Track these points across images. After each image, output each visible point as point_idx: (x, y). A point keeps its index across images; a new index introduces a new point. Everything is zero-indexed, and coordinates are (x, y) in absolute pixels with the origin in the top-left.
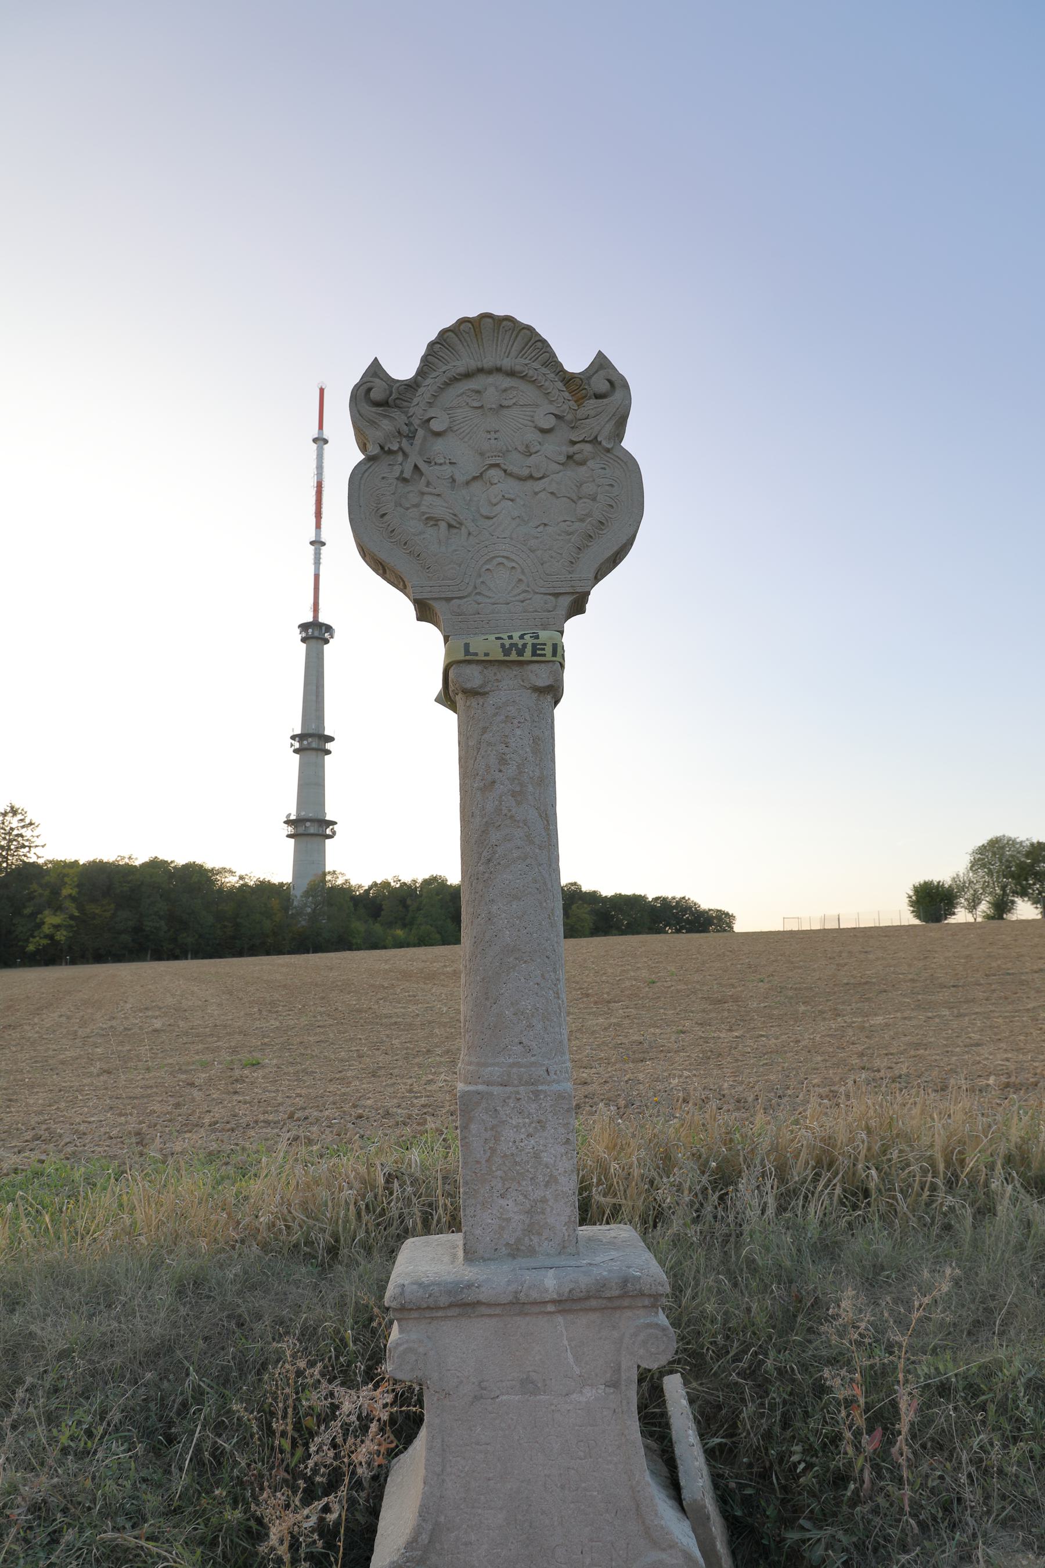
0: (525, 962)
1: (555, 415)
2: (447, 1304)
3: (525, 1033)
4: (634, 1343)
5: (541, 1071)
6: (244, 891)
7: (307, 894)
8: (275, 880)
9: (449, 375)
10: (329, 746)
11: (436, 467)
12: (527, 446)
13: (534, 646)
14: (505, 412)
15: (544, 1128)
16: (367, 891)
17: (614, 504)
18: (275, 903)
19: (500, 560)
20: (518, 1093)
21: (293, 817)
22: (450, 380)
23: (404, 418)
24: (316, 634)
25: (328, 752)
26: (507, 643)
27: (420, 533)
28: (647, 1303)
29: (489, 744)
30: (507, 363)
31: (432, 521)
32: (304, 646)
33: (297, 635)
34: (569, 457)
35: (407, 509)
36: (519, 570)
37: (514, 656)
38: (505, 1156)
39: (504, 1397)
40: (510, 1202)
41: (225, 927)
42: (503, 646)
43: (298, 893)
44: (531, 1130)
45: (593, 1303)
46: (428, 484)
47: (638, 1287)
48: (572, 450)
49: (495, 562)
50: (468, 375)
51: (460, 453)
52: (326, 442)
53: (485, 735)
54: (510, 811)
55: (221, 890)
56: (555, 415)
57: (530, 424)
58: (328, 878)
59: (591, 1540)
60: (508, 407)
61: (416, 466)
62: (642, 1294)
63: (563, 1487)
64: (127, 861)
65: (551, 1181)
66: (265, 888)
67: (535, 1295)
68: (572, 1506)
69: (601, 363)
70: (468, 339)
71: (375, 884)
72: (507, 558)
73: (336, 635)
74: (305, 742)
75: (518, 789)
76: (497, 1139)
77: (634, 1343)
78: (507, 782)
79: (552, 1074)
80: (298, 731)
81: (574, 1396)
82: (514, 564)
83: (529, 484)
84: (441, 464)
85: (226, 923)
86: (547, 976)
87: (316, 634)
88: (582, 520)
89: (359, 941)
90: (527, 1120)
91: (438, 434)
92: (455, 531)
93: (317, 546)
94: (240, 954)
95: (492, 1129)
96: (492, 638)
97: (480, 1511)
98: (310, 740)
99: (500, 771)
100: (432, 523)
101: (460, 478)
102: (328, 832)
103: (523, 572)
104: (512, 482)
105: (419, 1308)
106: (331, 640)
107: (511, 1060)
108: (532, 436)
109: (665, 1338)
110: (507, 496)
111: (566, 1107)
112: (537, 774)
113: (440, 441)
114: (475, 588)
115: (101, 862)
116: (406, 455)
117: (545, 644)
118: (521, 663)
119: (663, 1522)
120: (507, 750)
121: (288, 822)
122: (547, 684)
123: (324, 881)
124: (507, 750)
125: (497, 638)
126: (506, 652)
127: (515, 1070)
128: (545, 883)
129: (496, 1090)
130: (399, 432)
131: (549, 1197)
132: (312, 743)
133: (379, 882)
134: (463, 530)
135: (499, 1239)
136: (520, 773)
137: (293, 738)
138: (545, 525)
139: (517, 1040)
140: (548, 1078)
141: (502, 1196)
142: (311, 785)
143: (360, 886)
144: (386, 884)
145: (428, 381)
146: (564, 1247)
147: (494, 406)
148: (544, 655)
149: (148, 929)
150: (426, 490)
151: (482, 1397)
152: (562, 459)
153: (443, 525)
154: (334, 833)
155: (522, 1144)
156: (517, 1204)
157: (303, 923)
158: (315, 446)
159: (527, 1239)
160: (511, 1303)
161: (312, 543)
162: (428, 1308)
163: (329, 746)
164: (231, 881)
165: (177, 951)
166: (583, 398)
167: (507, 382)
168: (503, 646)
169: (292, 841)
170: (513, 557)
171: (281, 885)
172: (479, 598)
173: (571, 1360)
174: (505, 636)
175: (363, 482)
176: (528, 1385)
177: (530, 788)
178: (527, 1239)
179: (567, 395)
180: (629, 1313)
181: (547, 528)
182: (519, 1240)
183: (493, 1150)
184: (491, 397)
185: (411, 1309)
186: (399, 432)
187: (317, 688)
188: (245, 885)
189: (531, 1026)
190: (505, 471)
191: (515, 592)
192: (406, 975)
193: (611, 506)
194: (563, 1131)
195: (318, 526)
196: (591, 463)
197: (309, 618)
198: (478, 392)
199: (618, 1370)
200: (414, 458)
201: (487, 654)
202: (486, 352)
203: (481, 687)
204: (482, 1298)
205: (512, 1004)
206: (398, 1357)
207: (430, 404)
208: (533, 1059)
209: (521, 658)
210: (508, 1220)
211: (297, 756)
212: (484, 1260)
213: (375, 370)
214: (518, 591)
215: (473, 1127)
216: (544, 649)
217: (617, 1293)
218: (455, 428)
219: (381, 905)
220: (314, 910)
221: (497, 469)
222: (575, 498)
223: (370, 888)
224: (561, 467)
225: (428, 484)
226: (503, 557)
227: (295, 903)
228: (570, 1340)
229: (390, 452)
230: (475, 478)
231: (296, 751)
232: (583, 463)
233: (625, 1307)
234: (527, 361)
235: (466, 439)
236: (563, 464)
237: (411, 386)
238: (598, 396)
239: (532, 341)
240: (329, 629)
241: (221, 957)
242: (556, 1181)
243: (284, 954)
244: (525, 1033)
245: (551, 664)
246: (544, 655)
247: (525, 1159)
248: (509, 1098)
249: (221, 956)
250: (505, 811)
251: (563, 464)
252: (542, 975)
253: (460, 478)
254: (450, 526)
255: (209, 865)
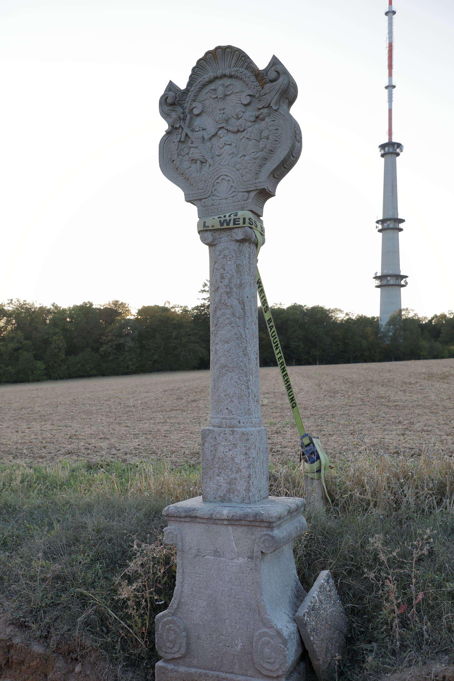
0: (230, 372)
1: (250, 95)
2: (184, 516)
3: (229, 404)
4: (259, 541)
5: (236, 422)
6: (349, 323)
7: (389, 323)
8: (369, 315)
9: (201, 83)
10: (401, 226)
11: (196, 133)
12: (237, 115)
13: (234, 219)
14: (228, 98)
15: (236, 447)
16: (430, 321)
17: (278, 139)
18: (369, 329)
19: (223, 177)
20: (225, 431)
21: (379, 274)
22: (203, 86)
23: (181, 110)
24: (391, 150)
25: (401, 230)
26: (222, 220)
27: (189, 168)
28: (266, 525)
29: (217, 269)
30: (227, 72)
31: (194, 161)
32: (383, 159)
33: (378, 152)
34: (257, 117)
35: (184, 156)
36: (232, 181)
37: (225, 226)
38: (219, 458)
39: (207, 557)
40: (221, 478)
41: (338, 345)
42: (220, 221)
43: (383, 323)
44: (231, 448)
45: (243, 522)
46: (192, 143)
47: (261, 518)
48: (258, 113)
49: (221, 178)
50: (211, 81)
51: (208, 123)
52: (394, 13)
53: (216, 265)
54: (225, 301)
55: (335, 323)
56: (250, 95)
57: (239, 102)
58: (403, 313)
59: (240, 619)
60: (229, 95)
61: (186, 134)
62: (262, 521)
63: (229, 596)
64: (279, 306)
65: (239, 471)
66: (363, 321)
67: (218, 516)
68: (233, 604)
69: (275, 62)
70: (211, 62)
71: (436, 316)
72: (227, 175)
73: (404, 149)
74: (385, 225)
75: (229, 290)
76: (216, 450)
77: (259, 541)
78: (224, 287)
79: (242, 423)
80: (381, 218)
81: (235, 560)
82: (229, 178)
83: (239, 134)
84: (198, 131)
85: (339, 343)
86: (241, 378)
87: (391, 150)
88: (262, 151)
89: (425, 354)
90: (229, 443)
91: (198, 115)
92: (204, 164)
93: (390, 88)
94: (348, 361)
95: (214, 446)
96: (216, 217)
97: (197, 600)
98: (389, 222)
99: (221, 282)
100: (194, 162)
101: (207, 137)
102: (403, 282)
103: (233, 182)
104: (231, 135)
105: (174, 516)
106: (401, 154)
107: (223, 416)
108: (240, 108)
109: (272, 541)
110: (226, 143)
111: (246, 438)
112: (238, 282)
113: (199, 119)
114: (212, 192)
115: (85, 311)
116: (182, 129)
117: (239, 219)
118: (230, 229)
119: (268, 617)
120: (224, 272)
121: (376, 278)
122: (241, 238)
123: (400, 315)
124: (224, 272)
125: (219, 218)
126: (222, 224)
127: (224, 421)
128: (241, 335)
129: (216, 429)
130: (180, 118)
131: (238, 477)
132: (390, 224)
133: (438, 315)
134: (208, 164)
135: (216, 493)
136: (230, 283)
137: (377, 222)
138: (245, 156)
139: (226, 408)
140: (239, 425)
141: (218, 475)
142: (390, 252)
143: (425, 318)
144: (443, 316)
145: (193, 88)
146: (244, 500)
147: (221, 96)
148: (239, 224)
149: (293, 346)
150: (191, 145)
151: (198, 555)
152: (253, 119)
153: (198, 162)
154: (407, 283)
155: (227, 454)
156: (224, 479)
157: (388, 342)
158: (387, 18)
159: (228, 495)
160: (208, 518)
161: (386, 88)
162: (177, 517)
163: (401, 226)
164: (341, 317)
165: (310, 360)
166: (265, 83)
167: (227, 81)
168: (220, 221)
169: (379, 289)
170: (229, 174)
171: (373, 318)
172: (214, 198)
173: (234, 545)
174: (222, 216)
175: (165, 145)
176: (216, 553)
177: (235, 290)
178: (228, 495)
179: (256, 83)
180: (259, 529)
181: (246, 157)
182: (225, 495)
183: (215, 455)
184: (220, 92)
185: (171, 516)
186: (180, 118)
187: (392, 187)
188: (350, 319)
189: (232, 401)
190: (227, 130)
191: (230, 193)
192: (431, 376)
193: (277, 141)
194: (244, 449)
195: (390, 75)
196: (267, 119)
197: (386, 140)
198: (215, 90)
199: (253, 552)
200: (186, 130)
201: (213, 226)
202: (223, 65)
203: (212, 242)
204: (198, 515)
205: (224, 391)
206: (166, 535)
207: (194, 100)
208: (232, 416)
209: (228, 227)
210: (221, 486)
211: (380, 234)
212: (210, 502)
213: (171, 87)
214: (231, 191)
215: (206, 444)
216: (239, 221)
217: (252, 519)
218: (205, 111)
219: (440, 330)
220: (394, 334)
221: (223, 129)
222: (258, 139)
223: (433, 319)
224: (253, 123)
225: (192, 143)
226: (225, 175)
227: (382, 330)
228: (234, 537)
229: (176, 128)
230: (213, 136)
231: (380, 231)
232: (263, 120)
233: (257, 526)
234: (238, 68)
235: (210, 116)
236: (254, 122)
237: (186, 91)
238: (272, 81)
239: (240, 57)
240: (399, 145)
241: (336, 363)
242: (241, 471)
243: (376, 362)
244: (229, 404)
245: (243, 228)
246: (239, 224)
247: (228, 460)
248: (221, 433)
249: (336, 363)
250: (223, 302)
251: (254, 122)
252: (239, 378)
253: (207, 137)
254: (202, 162)
255: (327, 308)
